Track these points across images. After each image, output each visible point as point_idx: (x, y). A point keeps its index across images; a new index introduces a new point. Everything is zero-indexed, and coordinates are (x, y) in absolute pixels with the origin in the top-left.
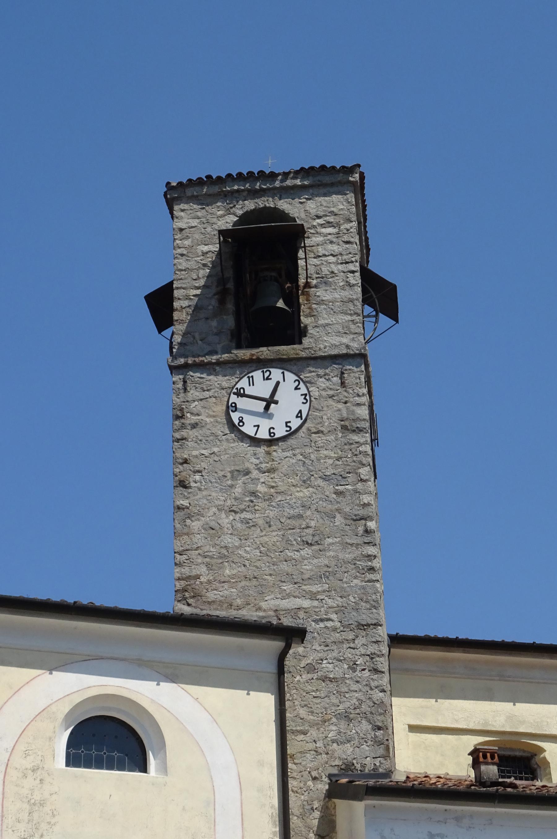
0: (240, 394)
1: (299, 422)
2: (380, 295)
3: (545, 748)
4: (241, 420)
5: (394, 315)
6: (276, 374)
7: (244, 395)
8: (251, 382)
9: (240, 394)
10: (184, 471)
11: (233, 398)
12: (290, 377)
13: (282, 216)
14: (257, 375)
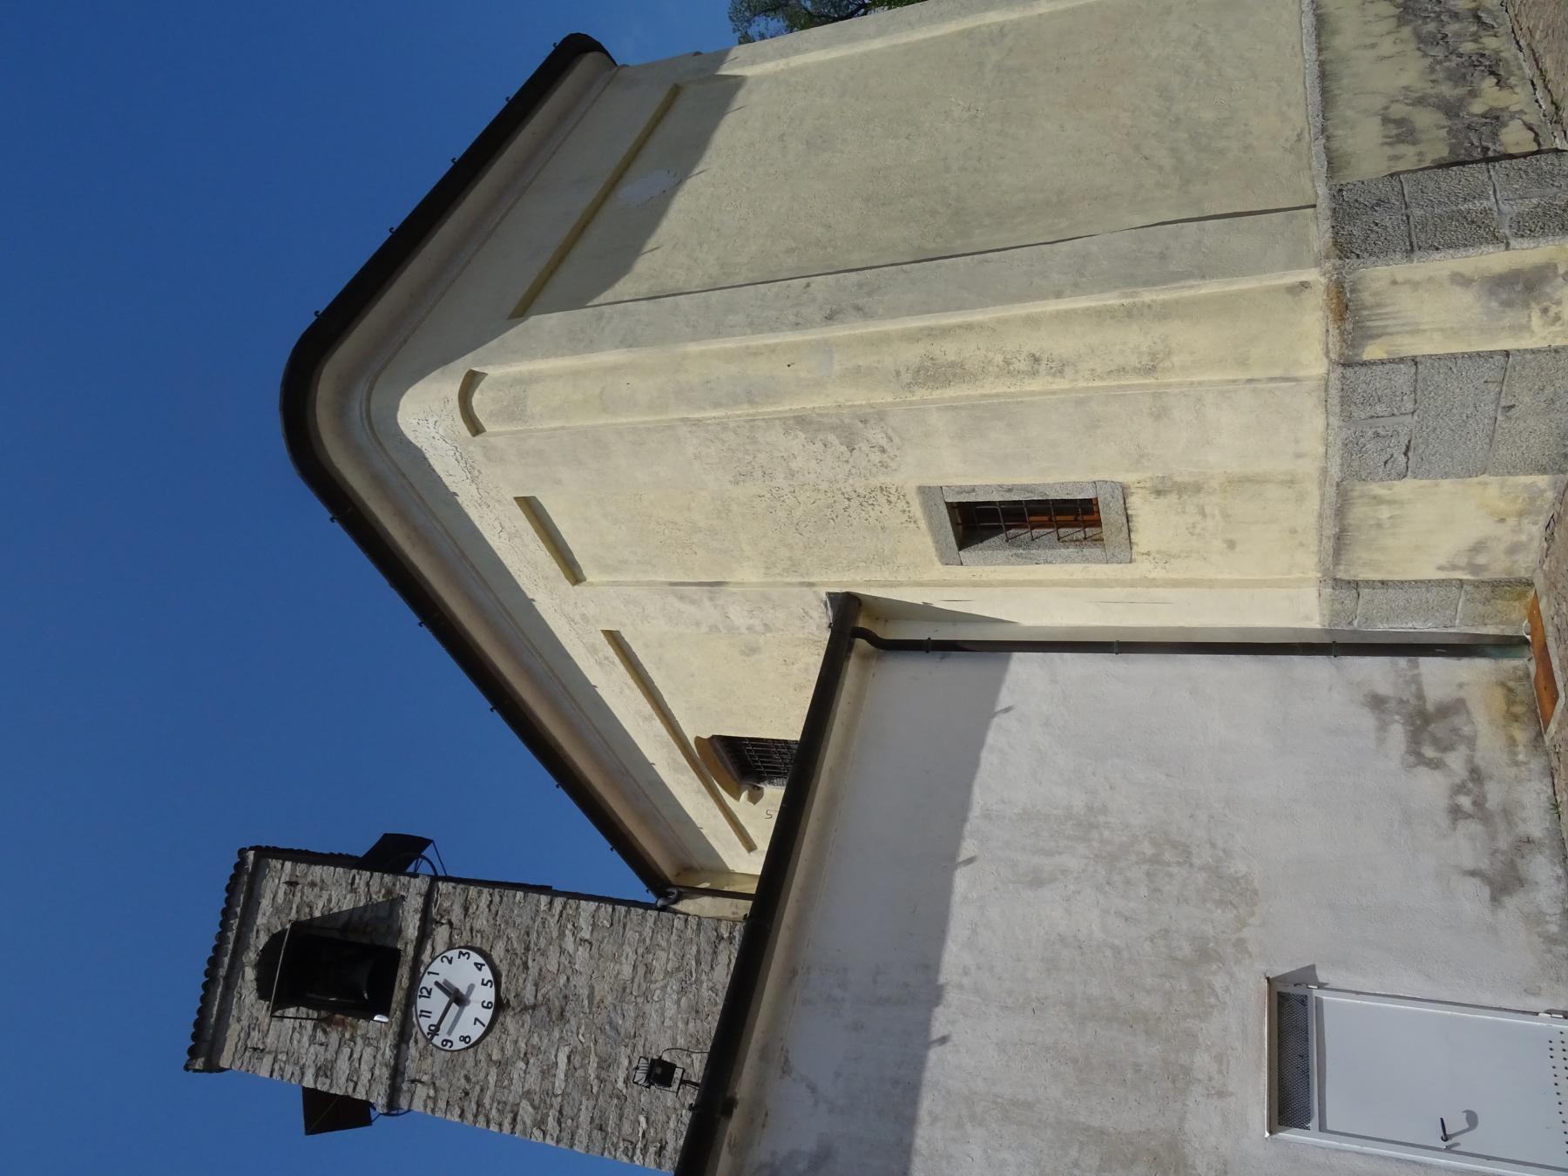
0: (435, 1030)
1: (486, 968)
2: (396, 854)
3: (1301, 965)
4: (463, 1039)
5: (425, 843)
6: (427, 981)
7: (438, 1027)
8: (426, 1014)
9: (435, 1030)
10: (1556, 1089)
11: (437, 1041)
12: (437, 966)
13: (276, 939)
14: (422, 1004)
